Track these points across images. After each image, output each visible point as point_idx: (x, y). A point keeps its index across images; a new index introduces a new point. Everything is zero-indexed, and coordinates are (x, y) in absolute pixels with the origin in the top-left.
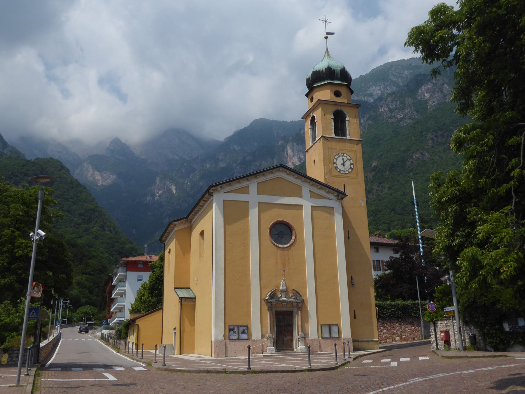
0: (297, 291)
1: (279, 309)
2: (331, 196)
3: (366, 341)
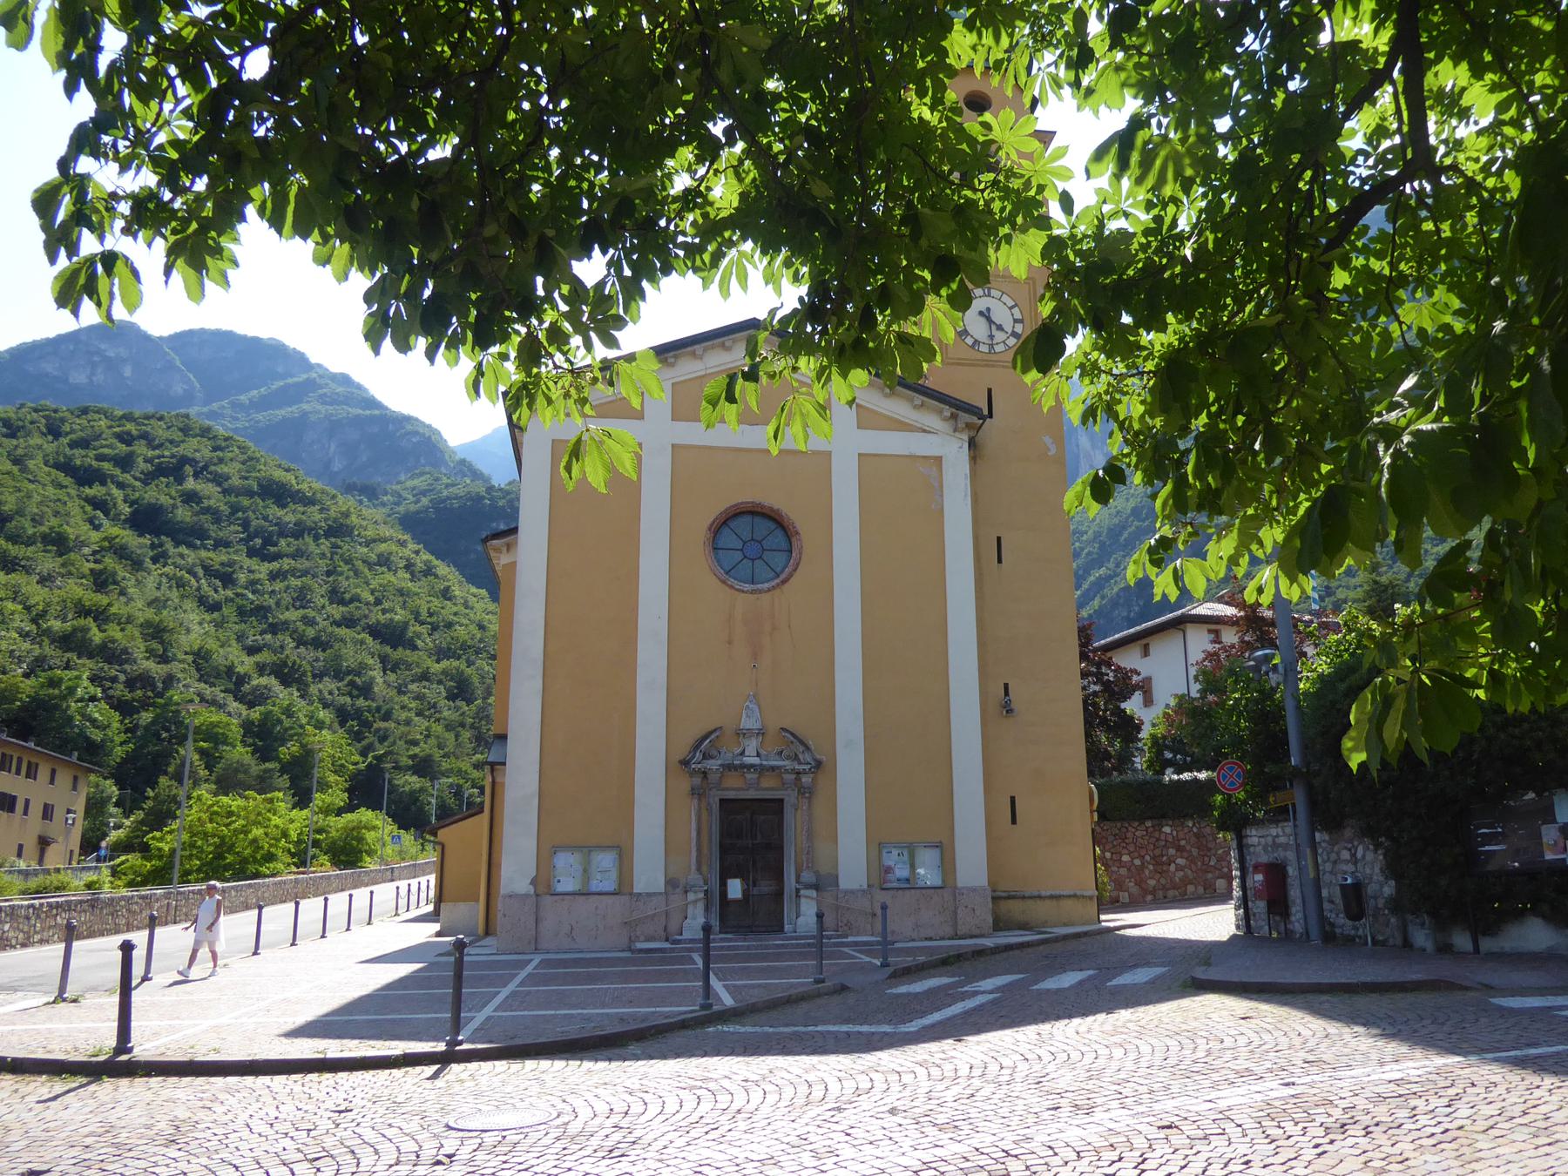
0: (792, 734)
1: (731, 795)
2: (932, 420)
3: (1052, 897)
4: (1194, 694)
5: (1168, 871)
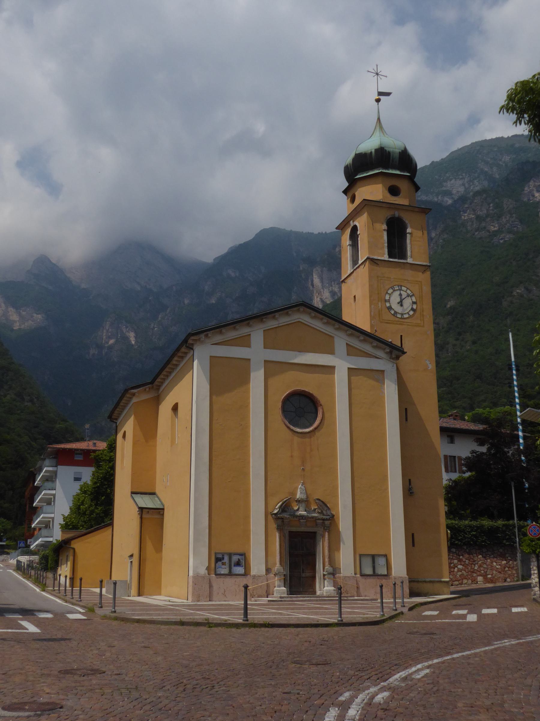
1: (294, 529)
4: (451, 484)
5: (454, 571)
